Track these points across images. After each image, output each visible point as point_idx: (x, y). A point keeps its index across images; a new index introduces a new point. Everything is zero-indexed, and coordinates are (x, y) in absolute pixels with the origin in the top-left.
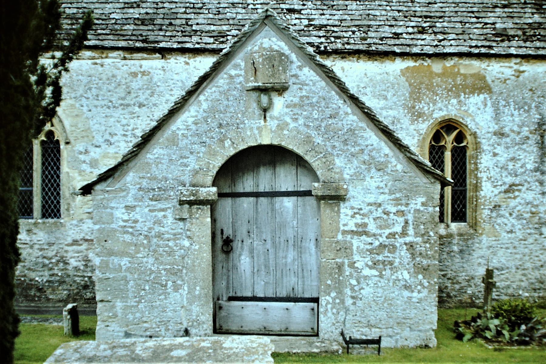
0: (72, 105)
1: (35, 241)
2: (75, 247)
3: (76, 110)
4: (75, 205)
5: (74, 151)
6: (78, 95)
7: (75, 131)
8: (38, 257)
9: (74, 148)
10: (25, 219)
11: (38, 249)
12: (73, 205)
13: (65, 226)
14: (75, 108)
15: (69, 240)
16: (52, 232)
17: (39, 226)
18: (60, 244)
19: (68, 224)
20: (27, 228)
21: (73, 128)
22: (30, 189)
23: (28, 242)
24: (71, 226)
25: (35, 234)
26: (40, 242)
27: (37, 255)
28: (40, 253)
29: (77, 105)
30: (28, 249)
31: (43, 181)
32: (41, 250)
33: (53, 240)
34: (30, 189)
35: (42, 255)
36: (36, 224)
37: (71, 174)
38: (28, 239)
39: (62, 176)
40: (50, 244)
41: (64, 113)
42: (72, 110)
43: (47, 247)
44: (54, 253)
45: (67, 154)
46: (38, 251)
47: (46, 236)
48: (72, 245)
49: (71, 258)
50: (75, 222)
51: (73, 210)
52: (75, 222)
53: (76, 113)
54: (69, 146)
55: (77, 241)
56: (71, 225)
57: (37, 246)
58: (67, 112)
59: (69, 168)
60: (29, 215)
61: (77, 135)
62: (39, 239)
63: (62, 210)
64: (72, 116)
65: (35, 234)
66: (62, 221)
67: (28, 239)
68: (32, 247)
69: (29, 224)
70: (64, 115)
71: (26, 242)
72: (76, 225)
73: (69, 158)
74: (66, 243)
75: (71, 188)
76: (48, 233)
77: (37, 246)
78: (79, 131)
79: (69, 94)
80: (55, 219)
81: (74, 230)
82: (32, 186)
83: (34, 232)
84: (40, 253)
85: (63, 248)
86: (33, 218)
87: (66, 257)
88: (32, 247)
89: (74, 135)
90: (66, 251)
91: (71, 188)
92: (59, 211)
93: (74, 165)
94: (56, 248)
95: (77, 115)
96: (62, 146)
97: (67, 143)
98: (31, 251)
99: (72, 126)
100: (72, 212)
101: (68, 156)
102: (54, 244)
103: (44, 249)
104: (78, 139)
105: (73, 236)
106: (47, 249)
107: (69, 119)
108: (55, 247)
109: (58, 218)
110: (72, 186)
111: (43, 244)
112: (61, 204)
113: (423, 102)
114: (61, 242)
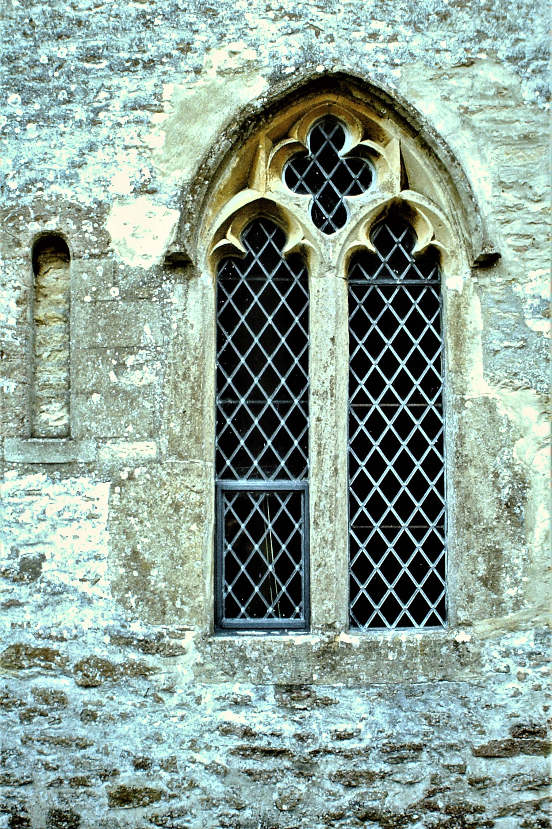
0: (501, 92)
1: (325, 740)
2: (521, 762)
3: (520, 113)
4: (528, 559)
5: (518, 301)
6: (529, 47)
7: (519, 208)
8: (340, 817)
9: (517, 289)
10: (268, 629)
11: (340, 776)
12: (514, 555)
13: (478, 660)
14: (520, 104)
15: (498, 728)
16: (411, 694)
17: (349, 663)
18: (451, 747)
19: (491, 651)
20: (286, 675)
21: (510, 197)
22: (294, 483)
23: (287, 744)
24: (509, 661)
25: (326, 703)
26: (346, 745)
27: (333, 807)
28: (349, 796)
29: (528, 93)
30: (290, 778)
31: (360, 446)
32: (350, 781)
33: (411, 730)
34: (294, 483)
35: (354, 804)
36: (328, 655)
37: (501, 412)
38: (289, 729)
39: (450, 424)
40: (398, 753)
41: (466, 124)
42: (503, 115)
43: (387, 768)
44: (418, 793)
45: (485, 311)
46: (338, 788)
47: (381, 714)
48: (509, 750)
49: (503, 812)
50: (524, 641)
51: (516, 583)
52: (524, 641)
53: (521, 127)
54: (491, 280)
55: (535, 731)
56: (506, 654)
57: (331, 765)
58: (476, 118)
59: (495, 381)
60: (285, 609)
61: (532, 229)
62: (342, 727)
63: (455, 581)
64: (507, 142)
65: (326, 703)
66: (462, 636)
67: (289, 729)
68: (304, 769)
69: (293, 655)
70: (468, 134)
71: (276, 744)
72: (530, 655)
73: (496, 334)
74: (480, 742)
75: (506, 474)
76: (388, 696)
77: (331, 765)
78: (536, 208)
79: (486, 44)
80: (418, 633)
81: (522, 678)
82: (298, 465)
83: (321, 692)
84: (349, 796)
85: (461, 769)
86: (306, 627)
87: (480, 810)
88: (304, 769)
89: (517, 227)
90: (479, 784)
91: (506, 474)
92: (435, 588)
93: (517, 367)
94: (429, 770)
95: (526, 138)
96: (455, 277)
97: (487, 262)
98: (302, 787)
99: (503, 186)
100: (512, 592)
101: (487, 323)
102: (418, 748)
103: (370, 777)
104: (535, 246)
105: (514, 707)
106: (383, 776)
107: (489, 151)
108: (422, 768)
109: (433, 622)
110: (509, 466)
111: (367, 750)
112: (450, 554)
113: (525, 601)
114: (453, 738)
